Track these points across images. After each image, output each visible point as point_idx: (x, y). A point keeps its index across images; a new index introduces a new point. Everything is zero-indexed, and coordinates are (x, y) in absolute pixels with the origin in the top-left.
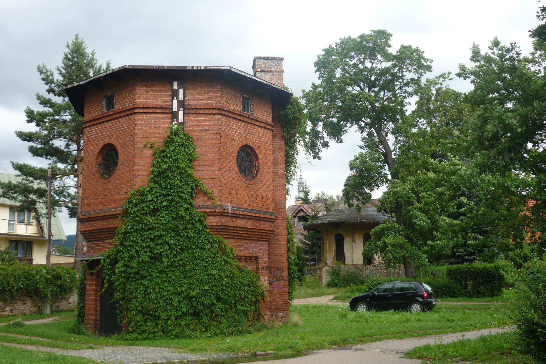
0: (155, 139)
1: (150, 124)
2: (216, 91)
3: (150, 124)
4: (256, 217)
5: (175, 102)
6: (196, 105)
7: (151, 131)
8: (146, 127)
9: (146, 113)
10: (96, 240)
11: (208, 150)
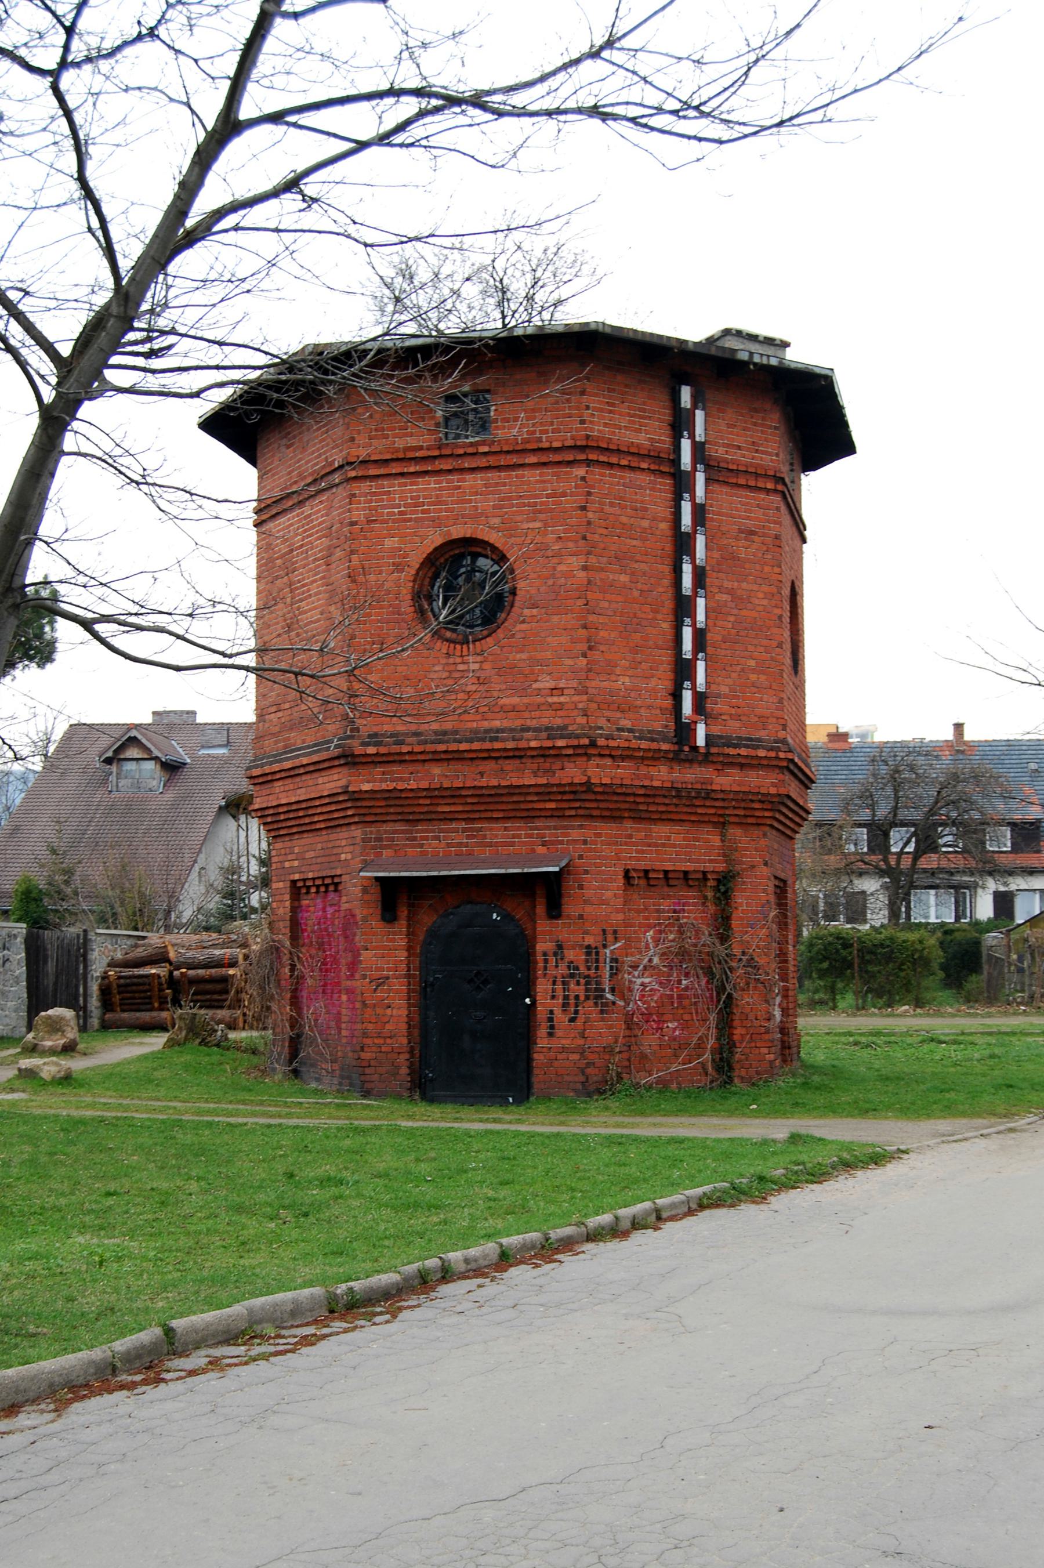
0: (634, 542)
1: (621, 499)
2: (770, 427)
3: (621, 499)
4: (505, 750)
5: (686, 445)
6: (727, 461)
7: (624, 519)
8: (612, 505)
9: (611, 465)
10: (408, 821)
11: (755, 587)
